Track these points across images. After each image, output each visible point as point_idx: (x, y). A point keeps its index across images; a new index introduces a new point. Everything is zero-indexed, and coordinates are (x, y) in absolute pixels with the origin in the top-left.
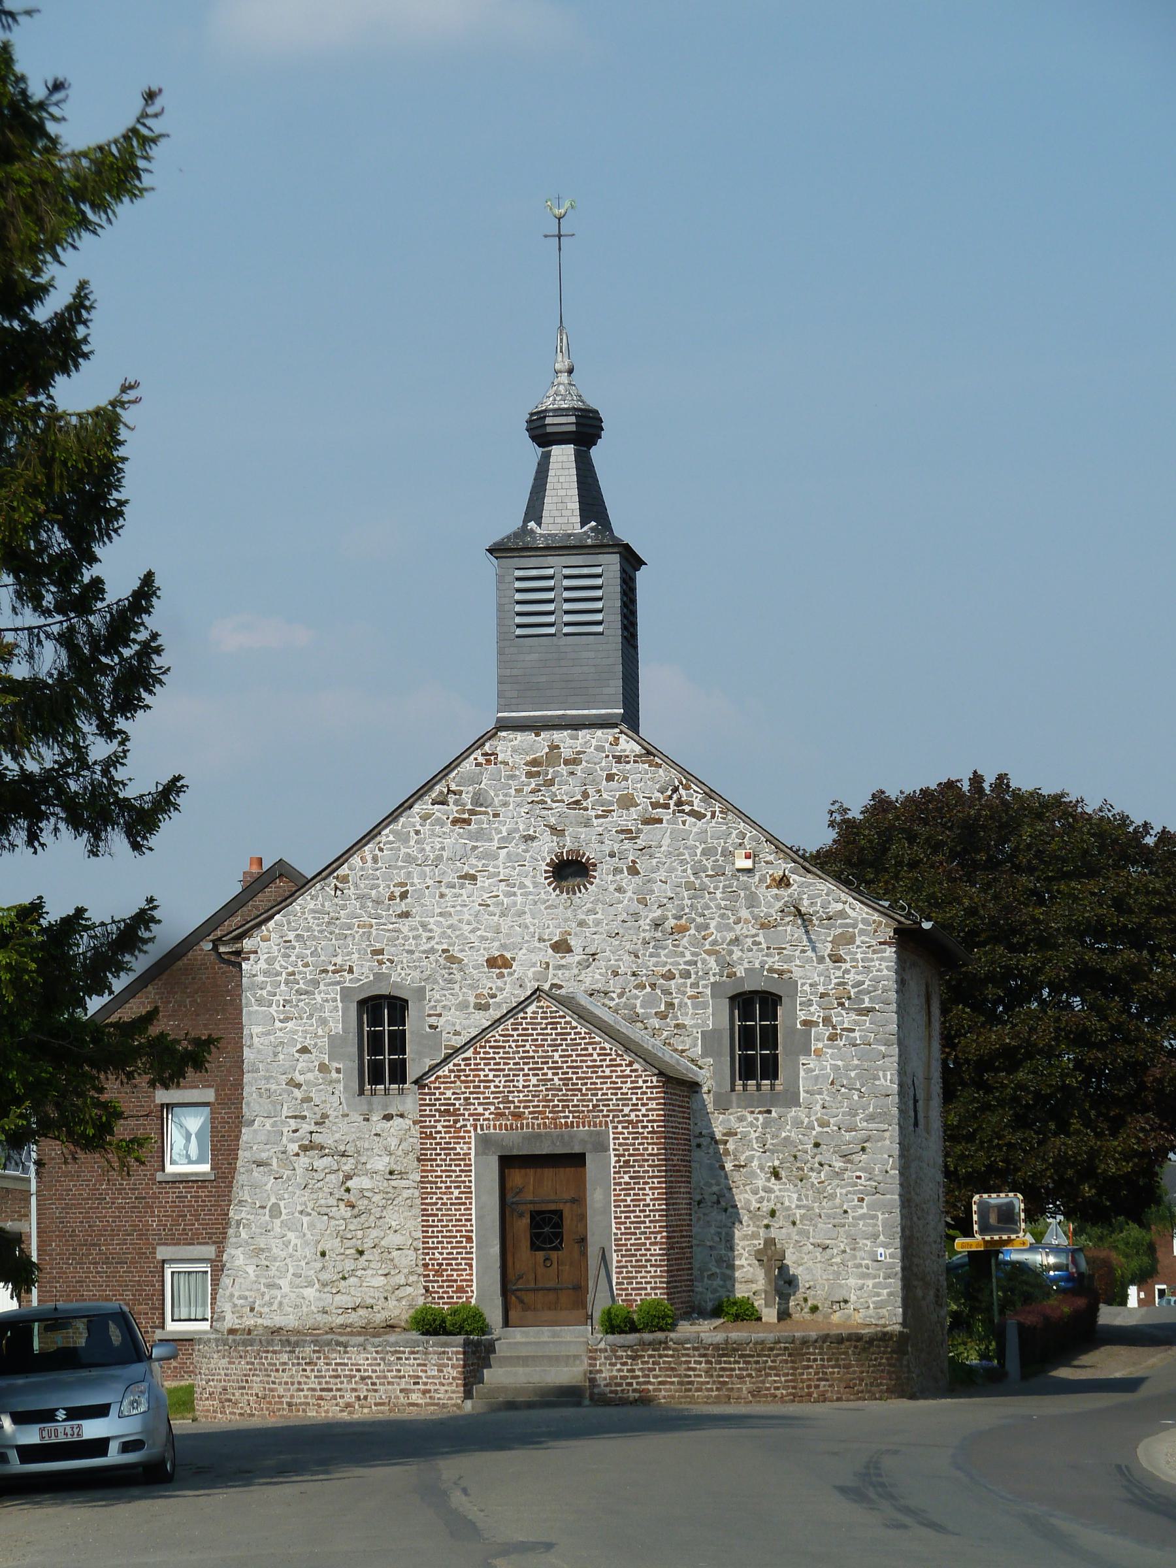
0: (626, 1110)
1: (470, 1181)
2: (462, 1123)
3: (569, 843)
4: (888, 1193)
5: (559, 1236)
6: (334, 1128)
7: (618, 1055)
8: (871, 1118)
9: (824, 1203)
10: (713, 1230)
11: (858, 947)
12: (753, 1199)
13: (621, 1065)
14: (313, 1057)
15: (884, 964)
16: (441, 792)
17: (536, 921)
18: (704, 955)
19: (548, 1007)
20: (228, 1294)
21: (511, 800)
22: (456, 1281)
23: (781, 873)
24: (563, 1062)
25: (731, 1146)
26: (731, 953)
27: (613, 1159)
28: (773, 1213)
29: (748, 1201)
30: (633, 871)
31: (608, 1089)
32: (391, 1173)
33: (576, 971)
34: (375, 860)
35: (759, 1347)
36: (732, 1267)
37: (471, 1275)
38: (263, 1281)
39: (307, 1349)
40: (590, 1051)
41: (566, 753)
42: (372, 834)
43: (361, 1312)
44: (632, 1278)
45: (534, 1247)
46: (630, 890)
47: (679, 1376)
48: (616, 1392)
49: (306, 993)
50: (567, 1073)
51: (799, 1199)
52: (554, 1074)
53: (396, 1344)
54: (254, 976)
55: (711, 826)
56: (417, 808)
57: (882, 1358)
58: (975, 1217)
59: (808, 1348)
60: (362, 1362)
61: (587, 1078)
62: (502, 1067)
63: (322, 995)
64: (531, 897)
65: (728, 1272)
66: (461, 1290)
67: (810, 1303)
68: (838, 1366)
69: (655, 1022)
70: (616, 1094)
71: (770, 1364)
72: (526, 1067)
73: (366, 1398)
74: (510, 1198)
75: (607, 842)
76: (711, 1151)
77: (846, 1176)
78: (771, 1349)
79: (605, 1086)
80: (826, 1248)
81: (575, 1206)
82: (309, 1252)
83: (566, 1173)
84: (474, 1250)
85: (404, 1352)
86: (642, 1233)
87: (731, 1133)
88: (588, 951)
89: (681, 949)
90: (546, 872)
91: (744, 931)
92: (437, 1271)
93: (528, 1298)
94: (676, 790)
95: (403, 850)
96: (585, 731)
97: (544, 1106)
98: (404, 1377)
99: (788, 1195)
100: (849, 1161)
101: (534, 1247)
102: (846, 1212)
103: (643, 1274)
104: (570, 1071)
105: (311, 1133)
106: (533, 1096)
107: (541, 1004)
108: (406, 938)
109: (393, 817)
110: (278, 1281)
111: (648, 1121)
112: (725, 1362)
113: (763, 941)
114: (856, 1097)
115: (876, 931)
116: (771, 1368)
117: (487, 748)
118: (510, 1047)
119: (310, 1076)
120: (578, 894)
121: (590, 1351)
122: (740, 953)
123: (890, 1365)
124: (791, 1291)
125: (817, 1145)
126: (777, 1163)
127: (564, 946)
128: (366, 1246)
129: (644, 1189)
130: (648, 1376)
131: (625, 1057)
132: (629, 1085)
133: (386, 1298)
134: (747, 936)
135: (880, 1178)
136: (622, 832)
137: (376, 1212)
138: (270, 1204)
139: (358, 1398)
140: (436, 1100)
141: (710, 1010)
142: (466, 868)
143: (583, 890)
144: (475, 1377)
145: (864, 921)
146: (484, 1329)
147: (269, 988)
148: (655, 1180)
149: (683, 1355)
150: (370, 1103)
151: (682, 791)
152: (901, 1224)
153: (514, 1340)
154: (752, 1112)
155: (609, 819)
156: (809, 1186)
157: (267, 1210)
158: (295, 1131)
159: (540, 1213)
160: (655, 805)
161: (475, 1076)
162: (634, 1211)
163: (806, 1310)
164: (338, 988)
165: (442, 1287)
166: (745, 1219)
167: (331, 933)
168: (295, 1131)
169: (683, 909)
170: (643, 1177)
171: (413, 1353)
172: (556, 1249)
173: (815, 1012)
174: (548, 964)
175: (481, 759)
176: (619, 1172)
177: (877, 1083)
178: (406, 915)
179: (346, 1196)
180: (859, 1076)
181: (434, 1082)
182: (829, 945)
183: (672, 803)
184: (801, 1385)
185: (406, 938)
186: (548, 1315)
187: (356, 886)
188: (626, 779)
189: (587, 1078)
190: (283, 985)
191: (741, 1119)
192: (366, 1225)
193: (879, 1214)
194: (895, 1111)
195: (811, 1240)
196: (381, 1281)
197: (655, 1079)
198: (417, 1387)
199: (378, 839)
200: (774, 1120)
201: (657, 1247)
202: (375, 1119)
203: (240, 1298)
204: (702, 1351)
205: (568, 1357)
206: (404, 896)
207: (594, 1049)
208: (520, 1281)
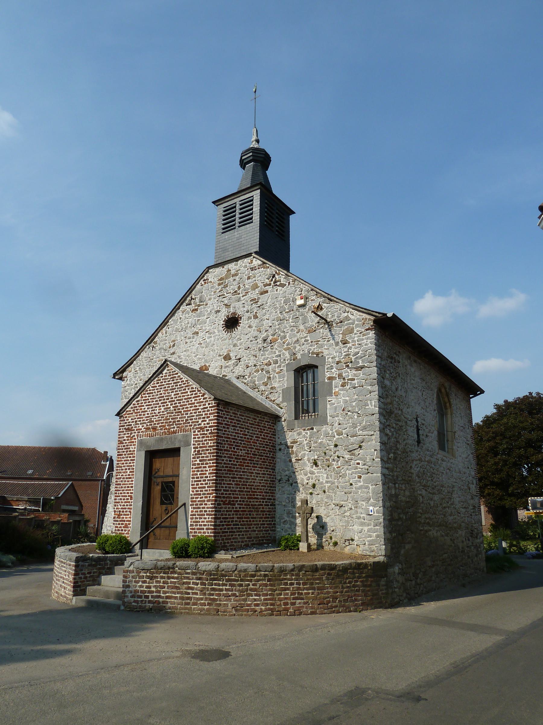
0: (200, 421)
3: (232, 310)
4: (375, 473)
7: (198, 391)
8: (364, 428)
10: (286, 496)
11: (355, 334)
12: (305, 478)
15: (369, 341)
18: (284, 351)
25: (294, 449)
26: (295, 348)
27: (193, 450)
28: (314, 486)
30: (256, 317)
33: (232, 368)
34: (166, 333)
40: (187, 390)
41: (233, 272)
42: (165, 323)
47: (181, 593)
51: (327, 478)
55: (289, 289)
57: (357, 581)
58: (530, 505)
59: (286, 575)
65: (293, 520)
67: (333, 540)
68: (314, 589)
69: (262, 388)
71: (251, 586)
75: (246, 306)
76: (286, 452)
87: (295, 442)
88: (237, 358)
89: (274, 350)
91: (302, 336)
94: (274, 276)
99: (322, 476)
100: (353, 454)
101: (162, 503)
102: (351, 484)
112: (216, 585)
114: (356, 417)
115: (364, 324)
116: (251, 590)
117: (205, 278)
118: (155, 392)
123: (364, 586)
125: (336, 446)
126: (316, 457)
127: (228, 357)
130: (159, 592)
132: (202, 407)
135: (370, 464)
141: (286, 378)
148: (211, 462)
149: (185, 578)
151: (277, 276)
152: (383, 491)
154: (304, 430)
163: (331, 544)
166: (301, 489)
169: (275, 330)
173: (335, 372)
174: (222, 366)
175: (203, 283)
178: (174, 353)
180: (357, 405)
181: (125, 415)
182: (341, 336)
184: (278, 603)
188: (255, 277)
191: (299, 434)
193: (370, 485)
194: (377, 423)
195: (333, 502)
197: (213, 402)
201: (210, 503)
204: (198, 576)
206: (174, 346)
207: (188, 389)
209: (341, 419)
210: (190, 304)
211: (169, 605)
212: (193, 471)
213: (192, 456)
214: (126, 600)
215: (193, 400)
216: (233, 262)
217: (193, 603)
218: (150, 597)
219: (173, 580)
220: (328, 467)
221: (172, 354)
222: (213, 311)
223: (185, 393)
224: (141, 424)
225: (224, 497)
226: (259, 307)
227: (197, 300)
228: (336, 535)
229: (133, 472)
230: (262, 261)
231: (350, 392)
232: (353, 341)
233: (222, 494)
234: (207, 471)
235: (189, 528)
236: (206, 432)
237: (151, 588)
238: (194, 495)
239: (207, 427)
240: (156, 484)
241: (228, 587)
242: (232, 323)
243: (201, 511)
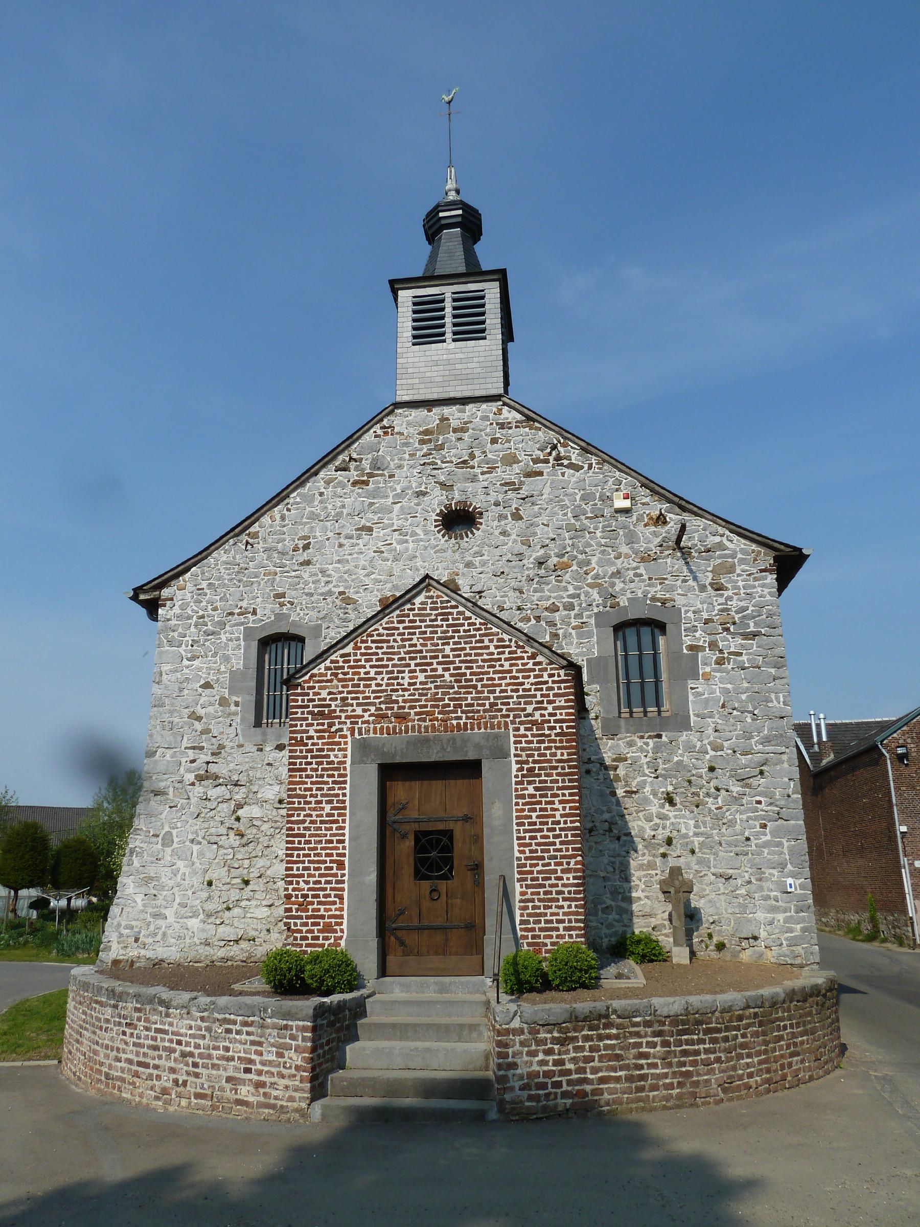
0: (530, 709)
1: (344, 795)
2: (337, 727)
3: (457, 496)
4: (792, 819)
5: (449, 861)
6: (229, 758)
7: (518, 647)
8: (766, 741)
9: (724, 830)
11: (739, 575)
12: (647, 826)
13: (522, 658)
14: (214, 692)
15: (766, 591)
16: (344, 461)
17: (426, 564)
18: (587, 588)
19: (438, 597)
20: (115, 923)
21: (406, 463)
22: (323, 917)
23: (658, 513)
24: (454, 656)
25: (621, 772)
26: (613, 585)
27: (515, 767)
28: (669, 841)
29: (642, 829)
30: (517, 516)
31: (508, 685)
32: (280, 802)
34: (283, 518)
35: (727, 1016)
36: (629, 900)
37: (342, 909)
39: (130, 1005)
40: (486, 643)
41: (454, 423)
42: (280, 497)
43: (244, 945)
44: (540, 915)
45: (419, 875)
48: (536, 1098)
49: (213, 633)
50: (460, 668)
52: (445, 670)
53: (224, 1009)
54: (169, 620)
56: (322, 474)
60: (183, 1031)
61: (483, 673)
62: (385, 663)
63: (227, 635)
64: (422, 543)
65: (624, 905)
66: (328, 928)
70: (517, 691)
71: (740, 1040)
72: (413, 663)
73: (185, 1083)
74: (391, 817)
75: (492, 493)
76: (601, 777)
77: (744, 801)
78: (740, 1018)
79: (503, 682)
80: (728, 878)
81: (467, 825)
82: (196, 881)
83: (457, 786)
84: (346, 878)
85: (235, 1023)
86: (550, 858)
87: (621, 759)
88: (475, 589)
89: (564, 584)
90: (436, 521)
91: (625, 564)
92: (301, 904)
93: (412, 939)
94: (554, 447)
95: (308, 509)
96: (471, 406)
97: (432, 706)
98: (233, 1059)
99: (684, 822)
100: (748, 786)
101: (419, 875)
102: (748, 839)
103: (554, 910)
104: (463, 665)
105: (208, 763)
106: (420, 695)
107: (431, 593)
108: (306, 583)
109: (300, 481)
110: (164, 911)
111: (556, 721)
112: (688, 1042)
113: (644, 572)
114: (749, 720)
115: (755, 560)
117: (385, 422)
118: (395, 641)
119: (211, 709)
120: (466, 539)
121: (499, 1033)
122: (622, 585)
124: (694, 926)
125: (712, 769)
126: (670, 788)
128: (252, 875)
129: (553, 803)
131: (527, 649)
132: (532, 680)
133: (268, 931)
134: (628, 569)
135: (783, 803)
136: (506, 484)
137: (264, 841)
138: (163, 832)
139: (176, 1082)
140: (309, 701)
142: (363, 522)
143: (470, 535)
144: (332, 1059)
145: (742, 551)
146: (353, 982)
147: (180, 630)
150: (264, 734)
153: (394, 997)
154: (642, 737)
155: (494, 474)
156: (706, 812)
157: (160, 839)
158: (193, 761)
159: (426, 833)
160: (536, 461)
161: (354, 674)
162: (541, 830)
164: (242, 628)
165: (306, 924)
166: (640, 847)
167: (239, 581)
168: (193, 761)
169: (565, 548)
170: (552, 789)
171: (246, 1024)
172: (445, 877)
173: (701, 637)
175: (380, 432)
176: (521, 783)
177: (770, 705)
178: (308, 563)
179: (236, 825)
180: (750, 699)
182: (710, 575)
183: (551, 458)
185: (306, 583)
186: (435, 961)
187: (265, 540)
188: (509, 441)
189: (483, 673)
190: (192, 627)
191: (631, 744)
192: (254, 854)
195: (713, 870)
196: (264, 912)
197: (562, 672)
198: (249, 1076)
199: (287, 501)
200: (665, 744)
201: (570, 876)
202: (268, 749)
203: (126, 927)
204: (657, 1027)
205: (461, 1026)
206: (306, 547)
207: (491, 641)
208: (402, 917)
209: (720, 722)
211: (606, 1096)
213: (514, 780)
214: (508, 1097)
216: (455, 404)
217: (650, 1085)
218: (564, 1084)
219: (609, 1042)
220: (697, 806)
221: (302, 564)
222: (410, 492)
223: (481, 648)
226: (523, 499)
228: (720, 931)
231: (734, 675)
232: (735, 587)
234: (557, 810)
235: (518, 927)
236: (547, 732)
237: (564, 1064)
238: (526, 859)
239: (549, 721)
240: (397, 835)
241: (707, 1046)
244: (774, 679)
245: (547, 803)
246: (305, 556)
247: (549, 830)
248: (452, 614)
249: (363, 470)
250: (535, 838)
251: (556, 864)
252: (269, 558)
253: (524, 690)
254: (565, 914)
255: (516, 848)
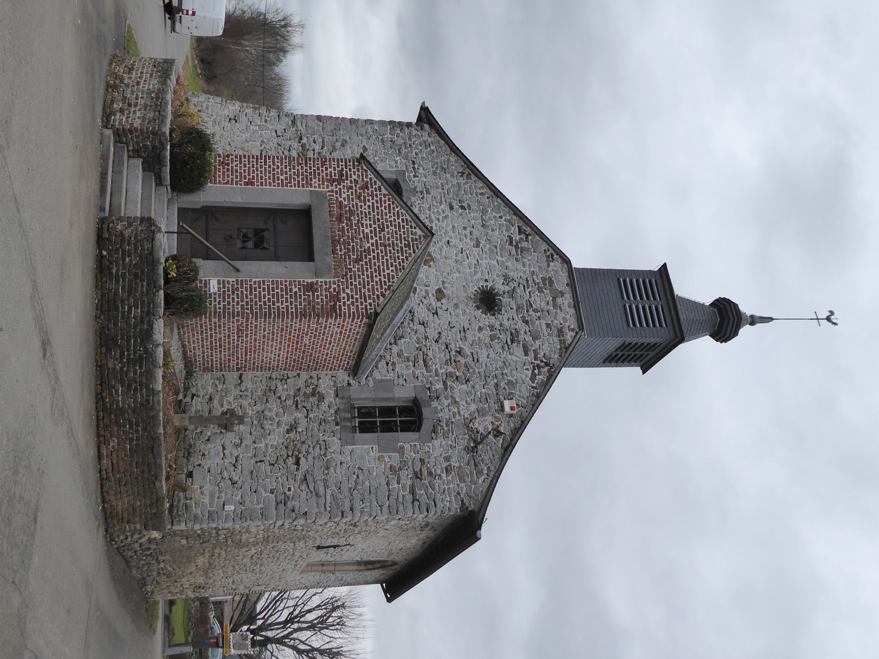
30: (493, 338)
34: (482, 194)
37: (220, 183)
38: (218, 118)
40: (391, 268)
46: (481, 335)
70: (360, 284)
88: (439, 310)
91: (462, 407)
94: (547, 364)
118: (390, 217)
132: (367, 293)
158: (314, 142)
160: (536, 352)
162: (269, 294)
168: (314, 142)
170: (296, 301)
173: (410, 454)
175: (548, 253)
178: (451, 208)
193: (261, 505)
206: (463, 208)
207: (392, 271)
210: (520, 232)
212: (281, 281)
215: (378, 279)
223: (387, 265)
224: (348, 196)
225: (247, 325)
227: (525, 244)
229: (282, 186)
230: (570, 345)
232: (449, 482)
233: (252, 323)
238: (251, 285)
242: (488, 301)
243: (229, 295)
244: (380, 506)
245: (287, 298)
246: (456, 207)
247: (269, 299)
248: (410, 249)
249: (520, 242)
250: (264, 290)
251: (247, 302)
252: (453, 186)
253: (360, 289)
254: (215, 306)
255: (258, 280)
